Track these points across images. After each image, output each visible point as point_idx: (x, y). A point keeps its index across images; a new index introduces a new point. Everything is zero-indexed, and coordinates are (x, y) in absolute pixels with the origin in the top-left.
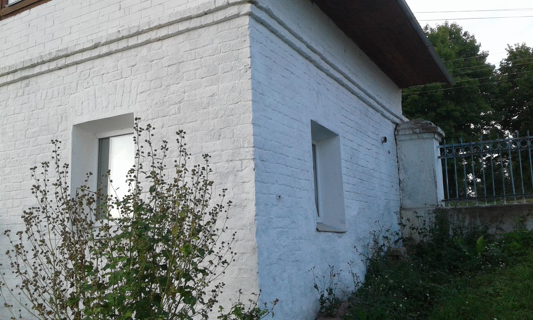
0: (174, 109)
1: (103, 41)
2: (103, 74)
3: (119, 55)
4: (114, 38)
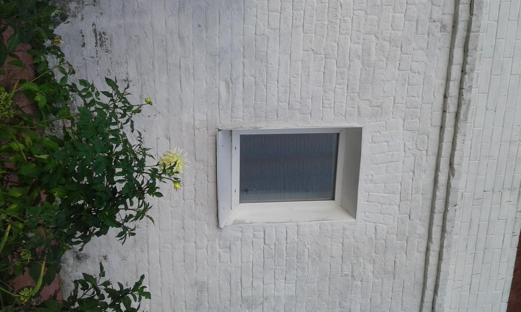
0: (347, 271)
1: (453, 182)
2: (414, 173)
3: (429, 196)
4: (451, 199)
